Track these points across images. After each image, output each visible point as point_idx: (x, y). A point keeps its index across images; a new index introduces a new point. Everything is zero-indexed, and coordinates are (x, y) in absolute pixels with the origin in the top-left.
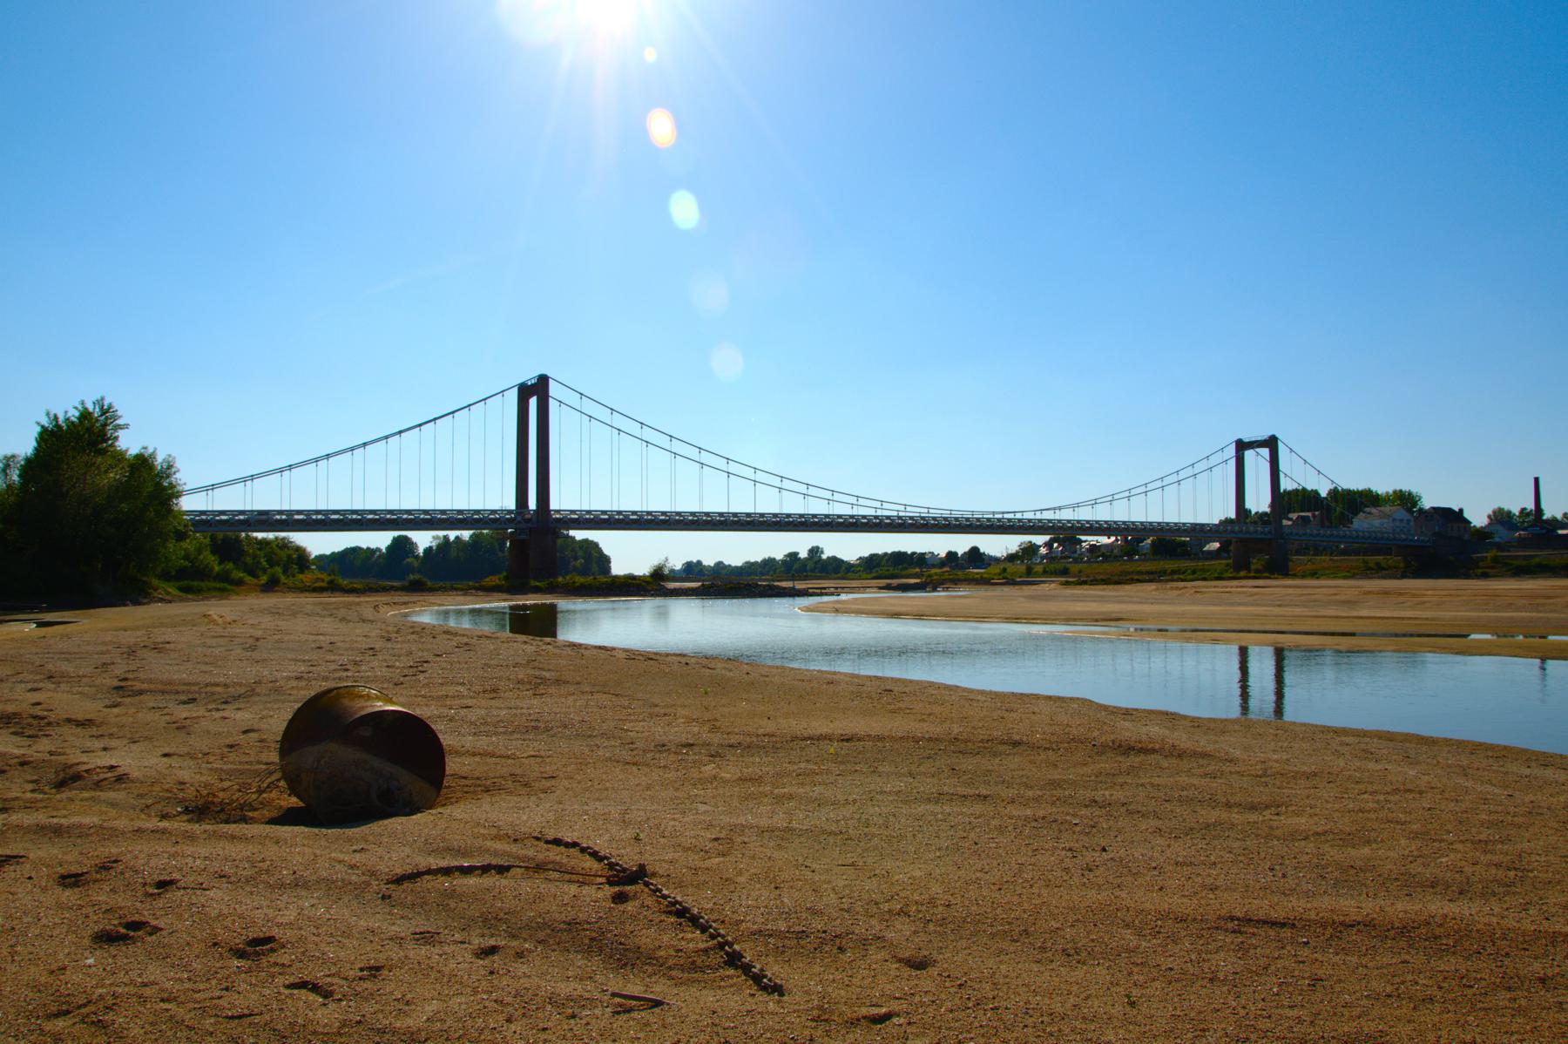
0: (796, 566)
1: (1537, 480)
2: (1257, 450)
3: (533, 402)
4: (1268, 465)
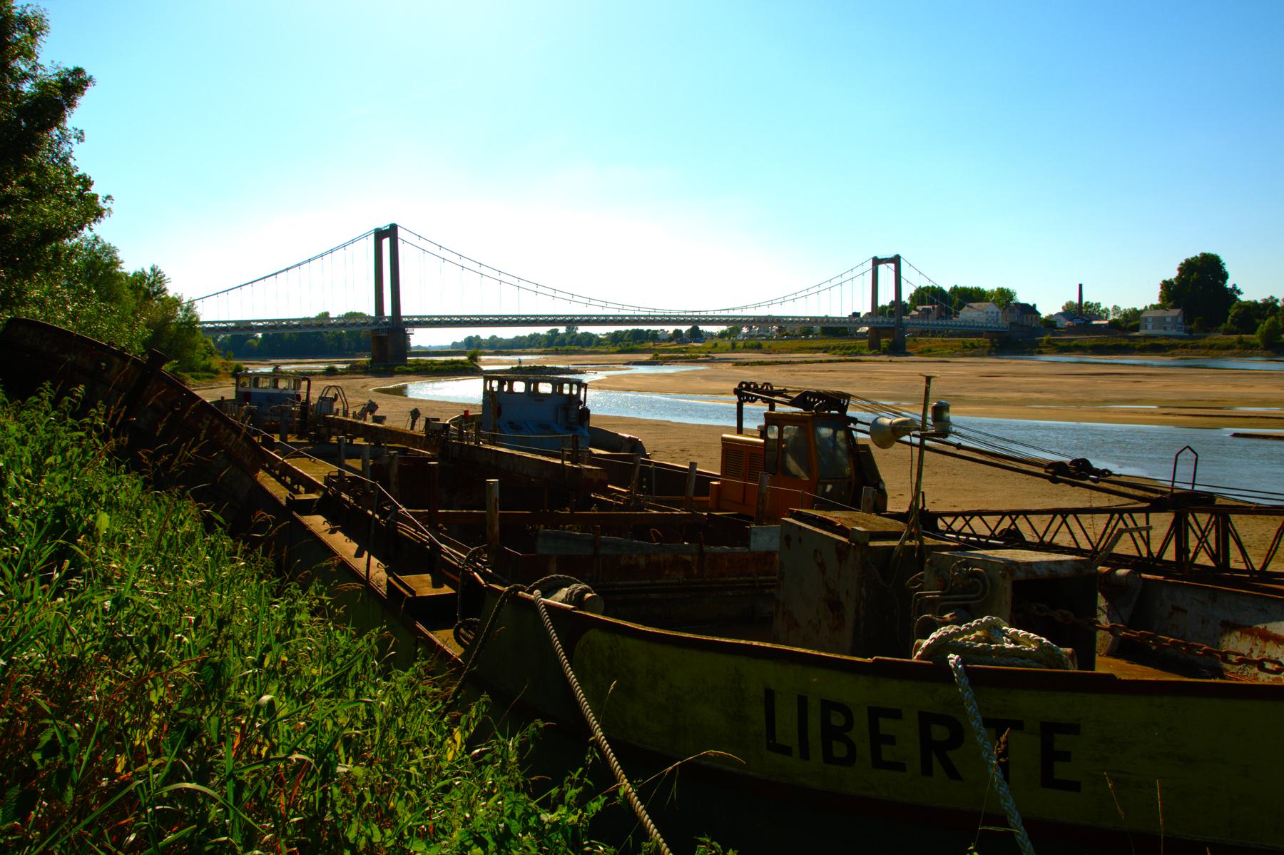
0: (557, 340)
1: (1081, 286)
2: (888, 264)
3: (386, 243)
4: (902, 275)
